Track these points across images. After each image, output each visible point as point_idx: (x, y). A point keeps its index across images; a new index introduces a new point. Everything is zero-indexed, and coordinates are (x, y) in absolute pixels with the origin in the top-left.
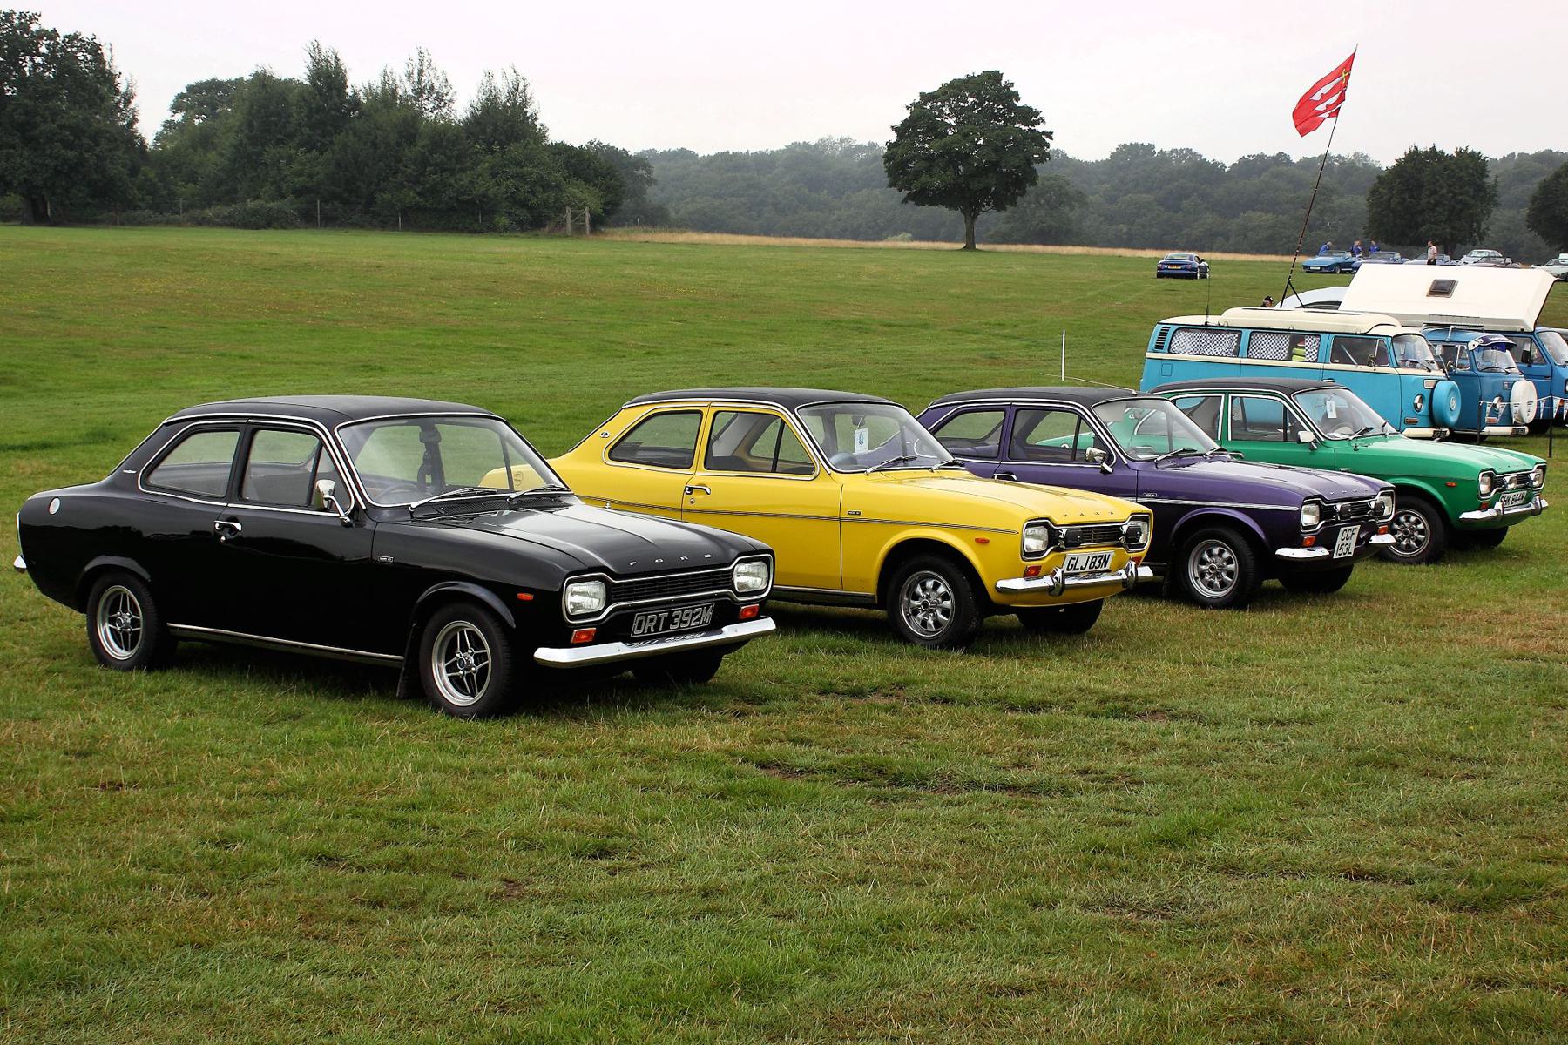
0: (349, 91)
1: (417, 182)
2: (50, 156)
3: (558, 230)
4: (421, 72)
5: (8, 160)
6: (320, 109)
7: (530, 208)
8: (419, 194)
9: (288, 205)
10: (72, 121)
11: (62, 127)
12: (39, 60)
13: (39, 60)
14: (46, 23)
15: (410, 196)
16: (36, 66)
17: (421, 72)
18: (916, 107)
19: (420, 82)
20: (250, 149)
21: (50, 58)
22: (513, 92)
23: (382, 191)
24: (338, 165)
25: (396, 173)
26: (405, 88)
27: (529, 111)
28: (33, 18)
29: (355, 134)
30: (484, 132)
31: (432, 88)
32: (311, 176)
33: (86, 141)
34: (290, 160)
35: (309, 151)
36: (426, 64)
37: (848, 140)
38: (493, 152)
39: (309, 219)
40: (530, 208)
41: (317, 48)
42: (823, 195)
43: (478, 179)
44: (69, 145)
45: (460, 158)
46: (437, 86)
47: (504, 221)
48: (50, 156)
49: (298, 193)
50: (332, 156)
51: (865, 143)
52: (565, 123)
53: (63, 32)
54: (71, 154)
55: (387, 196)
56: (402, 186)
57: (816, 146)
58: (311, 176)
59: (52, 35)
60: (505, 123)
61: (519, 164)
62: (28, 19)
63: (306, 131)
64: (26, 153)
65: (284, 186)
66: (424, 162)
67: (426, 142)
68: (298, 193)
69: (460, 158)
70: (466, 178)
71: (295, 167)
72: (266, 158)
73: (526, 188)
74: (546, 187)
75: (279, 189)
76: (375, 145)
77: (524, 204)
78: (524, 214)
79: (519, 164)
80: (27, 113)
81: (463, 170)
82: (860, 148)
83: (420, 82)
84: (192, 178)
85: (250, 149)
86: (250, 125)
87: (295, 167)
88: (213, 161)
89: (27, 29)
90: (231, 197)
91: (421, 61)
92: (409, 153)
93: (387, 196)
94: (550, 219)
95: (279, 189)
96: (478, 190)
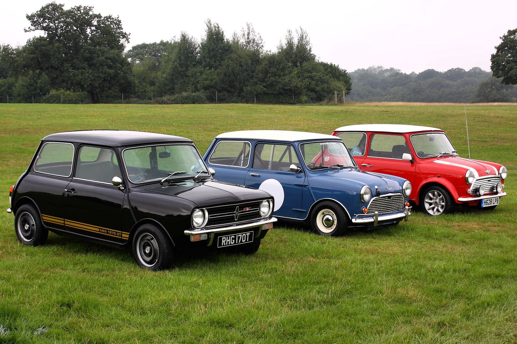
0: (225, 40)
1: (263, 81)
2: (102, 72)
3: (330, 101)
4: (249, 34)
5: (82, 75)
6: (213, 50)
7: (315, 92)
8: (264, 87)
9: (201, 94)
10: (111, 55)
11: (106, 58)
12: (93, 28)
13: (93, 28)
14: (96, 11)
15: (260, 88)
16: (92, 31)
17: (249, 34)
18: (505, 38)
19: (248, 38)
20: (180, 69)
21: (98, 27)
22: (302, 38)
23: (246, 86)
24: (225, 75)
25: (252, 77)
26: (242, 41)
27: (308, 47)
28: (90, 9)
29: (232, 60)
30: (291, 58)
31: (254, 40)
32: (212, 80)
33: (118, 65)
34: (201, 73)
35: (210, 69)
36: (251, 30)
37: (381, 67)
38: (296, 66)
39: (211, 100)
40: (315, 92)
41: (210, 22)
42: (378, 90)
43: (292, 79)
44: (110, 67)
45: (283, 69)
46: (256, 39)
47: (305, 98)
48: (102, 72)
49: (206, 88)
50: (224, 72)
51: (389, 68)
52: (323, 53)
53: (103, 15)
54: (111, 71)
55: (249, 88)
56: (256, 83)
57: (367, 70)
58: (212, 80)
59: (99, 16)
60: (297, 55)
61: (309, 72)
62: (87, 11)
63: (208, 60)
64: (90, 71)
65: (199, 86)
66: (266, 72)
67: (267, 62)
68: (206, 88)
69: (283, 69)
70: (287, 79)
71: (204, 76)
72: (189, 73)
73: (314, 82)
74: (323, 82)
75: (196, 87)
76: (241, 66)
77: (313, 90)
78: (313, 95)
79: (309, 72)
80: (90, 52)
81: (284, 75)
82: (386, 70)
83: (248, 38)
84: (152, 84)
85: (180, 69)
86: (180, 59)
87: (204, 76)
88: (161, 76)
89: (87, 14)
90: (172, 91)
91: (249, 28)
92: (259, 68)
93: (249, 88)
94: (325, 97)
95: (196, 87)
96: (293, 84)
